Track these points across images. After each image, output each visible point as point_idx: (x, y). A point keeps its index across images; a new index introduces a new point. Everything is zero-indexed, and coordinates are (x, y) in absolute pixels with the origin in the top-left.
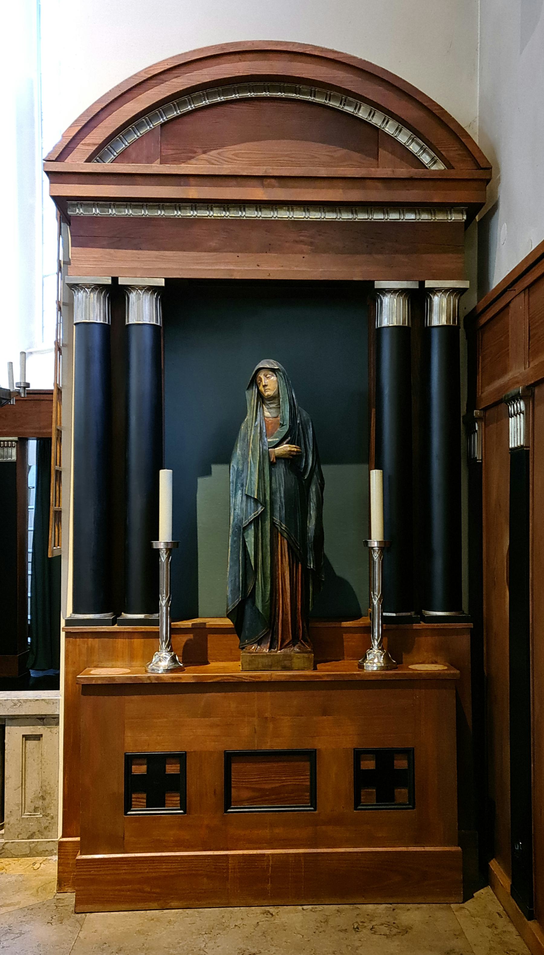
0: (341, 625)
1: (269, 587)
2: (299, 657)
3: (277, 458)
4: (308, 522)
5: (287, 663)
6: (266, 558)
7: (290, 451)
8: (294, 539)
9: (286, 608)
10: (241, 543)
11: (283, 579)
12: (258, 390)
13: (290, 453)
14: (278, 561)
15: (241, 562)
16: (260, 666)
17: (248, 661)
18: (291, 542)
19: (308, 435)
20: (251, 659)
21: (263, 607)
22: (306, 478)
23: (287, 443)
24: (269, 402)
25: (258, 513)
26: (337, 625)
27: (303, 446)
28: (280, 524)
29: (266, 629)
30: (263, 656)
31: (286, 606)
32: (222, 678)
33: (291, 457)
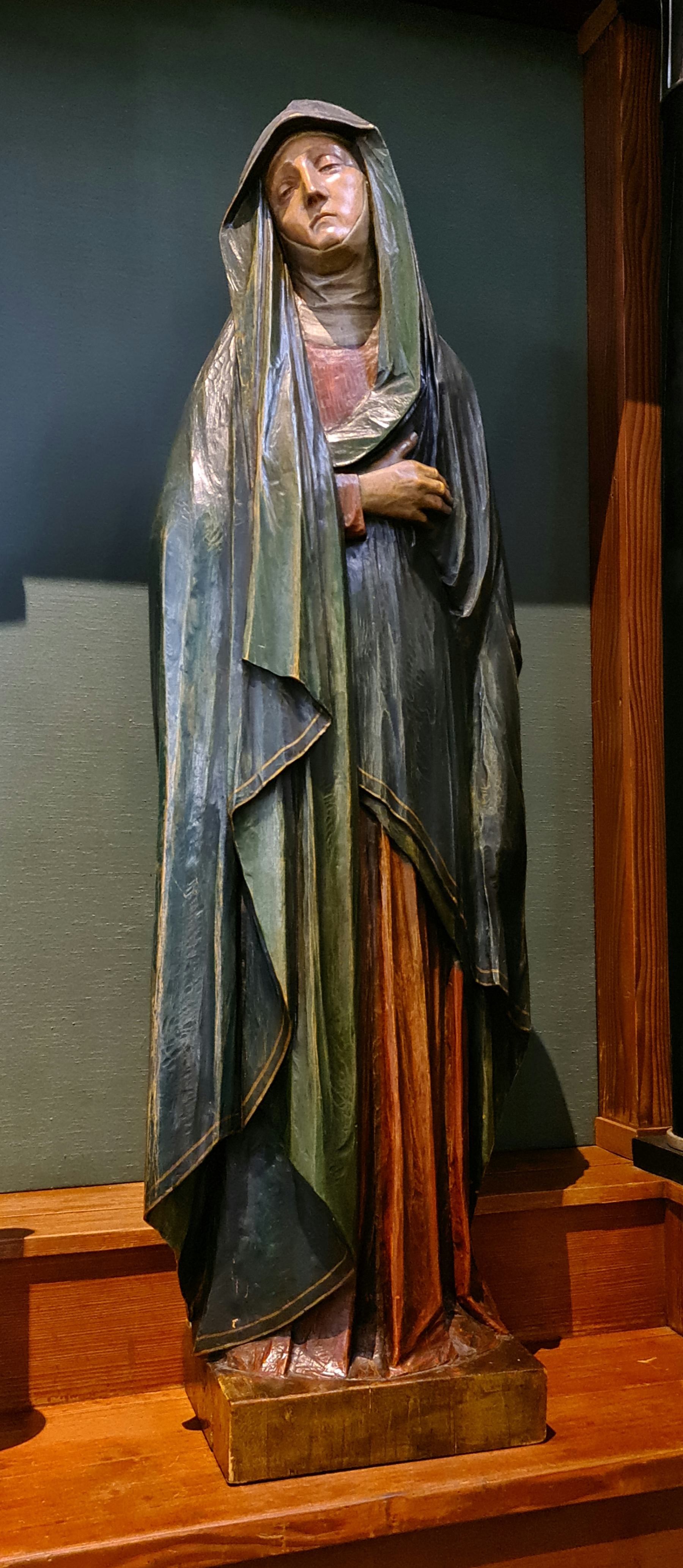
0: (561, 1196)
1: (354, 1078)
2: (486, 1388)
3: (372, 515)
4: (474, 794)
5: (436, 1421)
6: (336, 949)
7: (422, 487)
8: (440, 865)
9: (415, 1165)
10: (220, 882)
11: (403, 1037)
12: (279, 230)
13: (421, 500)
14: (382, 958)
15: (218, 970)
16: (319, 1451)
17: (264, 1432)
18: (427, 878)
19: (468, 439)
20: (276, 1421)
21: (331, 1168)
22: (466, 613)
23: (407, 456)
24: (324, 282)
25: (302, 744)
26: (540, 1199)
27: (457, 477)
28: (390, 798)
29: (338, 1274)
30: (328, 1404)
31: (415, 1156)
32: (158, 1555)
33: (423, 518)
